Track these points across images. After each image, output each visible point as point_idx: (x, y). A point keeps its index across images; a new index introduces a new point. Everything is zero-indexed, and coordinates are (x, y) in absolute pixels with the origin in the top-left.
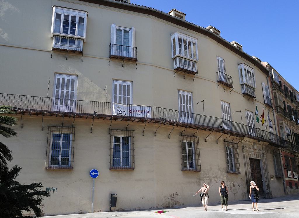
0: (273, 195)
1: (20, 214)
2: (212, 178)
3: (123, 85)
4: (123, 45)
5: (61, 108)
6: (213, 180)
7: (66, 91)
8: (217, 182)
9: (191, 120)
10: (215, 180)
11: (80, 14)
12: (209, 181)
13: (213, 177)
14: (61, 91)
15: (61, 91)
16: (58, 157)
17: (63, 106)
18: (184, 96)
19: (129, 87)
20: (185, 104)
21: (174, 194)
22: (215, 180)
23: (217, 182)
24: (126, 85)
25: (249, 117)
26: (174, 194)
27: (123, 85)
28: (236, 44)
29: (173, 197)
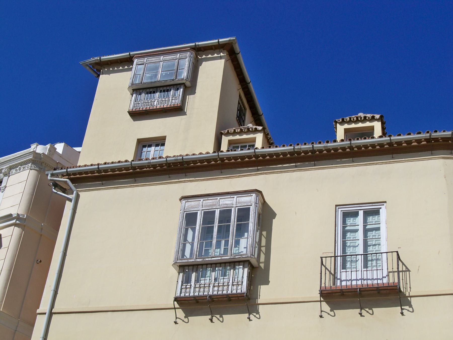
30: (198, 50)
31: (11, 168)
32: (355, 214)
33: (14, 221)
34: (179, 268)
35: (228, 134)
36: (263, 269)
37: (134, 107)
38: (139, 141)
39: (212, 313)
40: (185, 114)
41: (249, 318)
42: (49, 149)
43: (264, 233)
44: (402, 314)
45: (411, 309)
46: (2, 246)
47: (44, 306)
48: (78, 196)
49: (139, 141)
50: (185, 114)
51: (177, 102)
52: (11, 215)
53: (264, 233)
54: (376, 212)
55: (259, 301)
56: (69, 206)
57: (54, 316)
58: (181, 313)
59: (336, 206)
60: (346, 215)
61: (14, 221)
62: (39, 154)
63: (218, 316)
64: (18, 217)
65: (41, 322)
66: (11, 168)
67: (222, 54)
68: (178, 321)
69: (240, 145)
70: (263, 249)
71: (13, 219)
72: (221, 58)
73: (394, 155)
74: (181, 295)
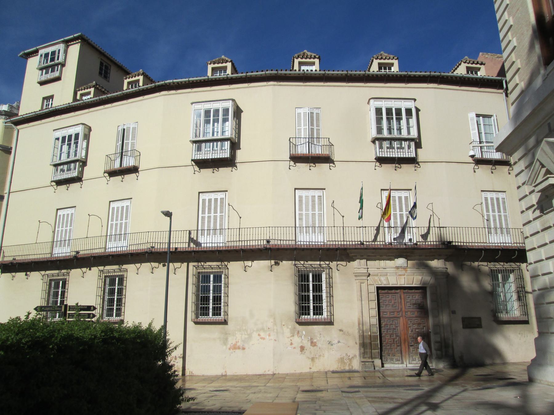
0: (419, 356)
1: (418, 336)
2: (254, 331)
3: (398, 197)
4: (315, 139)
5: (208, 239)
6: (255, 335)
7: (312, 212)
8: (263, 339)
9: (110, 244)
10: (259, 335)
11: (205, 106)
12: (246, 336)
13: (255, 329)
14: (400, 214)
15: (400, 214)
16: (215, 296)
17: (211, 236)
18: (492, 199)
19: (320, 197)
20: (402, 212)
21: (176, 357)
22: (259, 335)
23: (263, 339)
24: (217, 198)
25: (111, 232)
26: (176, 357)
27: (398, 197)
28: (142, 76)
29: (175, 360)
47: (7, 191)
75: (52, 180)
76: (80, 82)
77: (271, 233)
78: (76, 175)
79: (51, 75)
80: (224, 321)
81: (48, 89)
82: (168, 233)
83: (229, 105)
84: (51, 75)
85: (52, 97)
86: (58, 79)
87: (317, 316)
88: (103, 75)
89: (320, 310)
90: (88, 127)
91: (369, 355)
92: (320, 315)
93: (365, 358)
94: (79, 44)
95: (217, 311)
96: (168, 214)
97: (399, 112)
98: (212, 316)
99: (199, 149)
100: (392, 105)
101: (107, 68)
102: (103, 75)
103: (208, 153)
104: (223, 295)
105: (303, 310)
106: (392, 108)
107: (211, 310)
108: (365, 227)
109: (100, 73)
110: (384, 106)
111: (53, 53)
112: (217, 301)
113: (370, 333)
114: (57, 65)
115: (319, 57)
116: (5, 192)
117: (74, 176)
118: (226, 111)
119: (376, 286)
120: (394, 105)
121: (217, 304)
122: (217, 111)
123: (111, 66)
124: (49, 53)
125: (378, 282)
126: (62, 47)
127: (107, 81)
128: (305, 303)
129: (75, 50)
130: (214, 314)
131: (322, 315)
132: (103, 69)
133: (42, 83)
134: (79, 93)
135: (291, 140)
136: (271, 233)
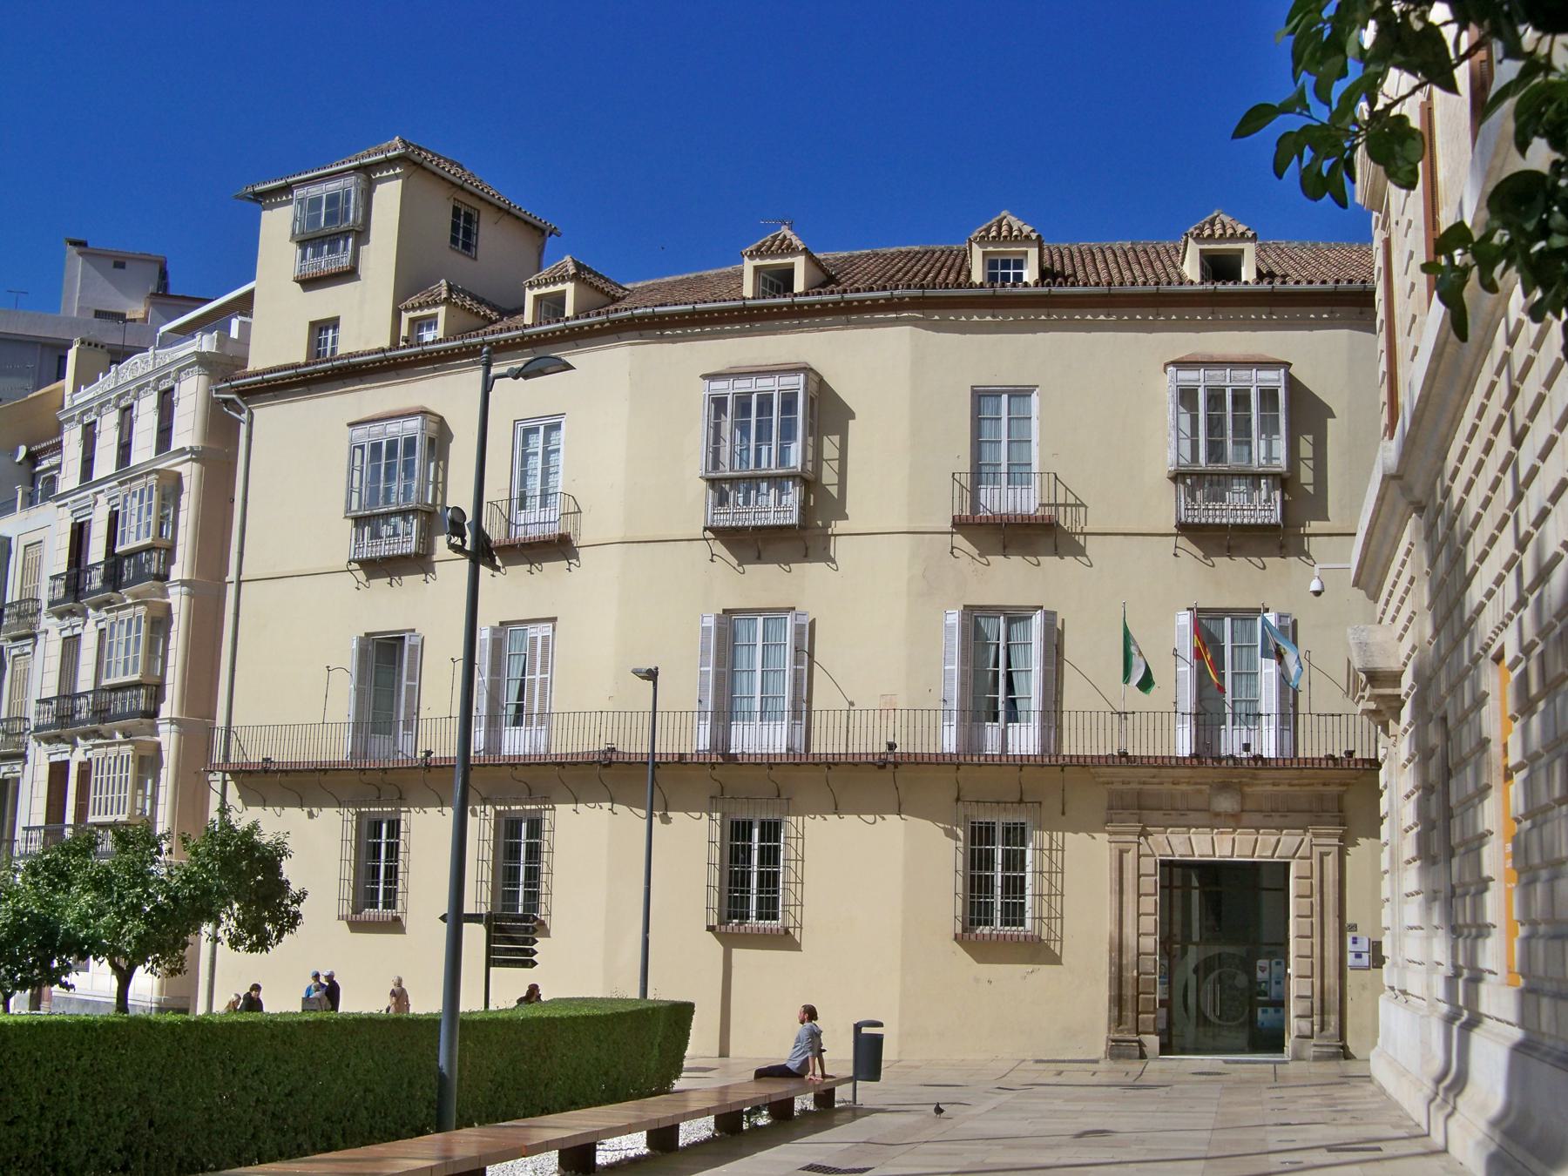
30: (366, 169)
31: (180, 370)
32: (536, 430)
33: (189, 456)
34: (1472, 620)
35: (407, 310)
36: (1465, 571)
37: (301, 271)
38: (313, 324)
39: (390, 576)
40: (358, 279)
41: (425, 580)
42: (218, 339)
43: (441, 463)
44: (569, 570)
45: (578, 564)
46: (978, 962)
47: (232, 575)
48: (251, 414)
49: (313, 324)
50: (358, 279)
51: (345, 261)
52: (184, 448)
53: (441, 463)
54: (557, 427)
55: (435, 558)
56: (243, 428)
57: (243, 584)
58: (361, 575)
59: (515, 421)
60: (527, 432)
61: (189, 456)
62: (204, 353)
63: (397, 578)
64: (192, 450)
65: (231, 591)
66: (180, 370)
67: (398, 170)
68: (360, 585)
69: (426, 322)
70: (440, 485)
71: (187, 453)
72: (397, 177)
73: (579, 342)
74: (1273, 839)
75: (352, 557)
76: (410, 285)
77: (898, 724)
78: (413, 550)
79: (326, 263)
80: (783, 933)
81: (325, 302)
82: (648, 717)
83: (797, 382)
84: (326, 263)
85: (334, 323)
86: (349, 274)
87: (1014, 928)
88: (460, 242)
89: (986, 914)
90: (437, 419)
91: (1130, 1024)
92: (986, 924)
93: (1122, 1031)
94: (400, 181)
95: (769, 909)
96: (652, 675)
97: (1241, 398)
98: (1001, 925)
99: (722, 500)
100: (1225, 381)
101: (469, 219)
102: (460, 242)
103: (741, 515)
104: (781, 869)
105: (976, 912)
106: (1224, 390)
107: (999, 889)
108: (1134, 713)
109: (454, 240)
110: (1203, 385)
111: (333, 200)
112: (768, 886)
113: (1135, 973)
114: (345, 234)
115: (1039, 237)
116: (227, 579)
117: (409, 550)
118: (789, 401)
119: (1159, 858)
120: (1228, 380)
121: (768, 892)
122: (765, 401)
123: (479, 212)
124: (320, 199)
125: (1164, 850)
126: (350, 184)
127: (471, 257)
128: (986, 897)
129: (388, 197)
130: (1005, 923)
131: (992, 925)
132: (460, 214)
133: (309, 283)
134: (405, 317)
135: (957, 476)
136: (898, 724)
